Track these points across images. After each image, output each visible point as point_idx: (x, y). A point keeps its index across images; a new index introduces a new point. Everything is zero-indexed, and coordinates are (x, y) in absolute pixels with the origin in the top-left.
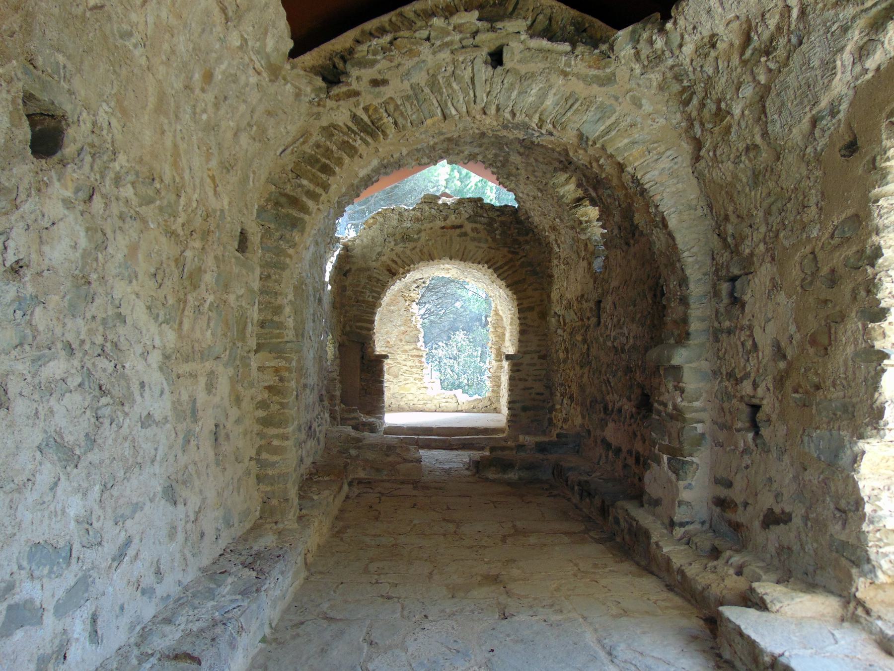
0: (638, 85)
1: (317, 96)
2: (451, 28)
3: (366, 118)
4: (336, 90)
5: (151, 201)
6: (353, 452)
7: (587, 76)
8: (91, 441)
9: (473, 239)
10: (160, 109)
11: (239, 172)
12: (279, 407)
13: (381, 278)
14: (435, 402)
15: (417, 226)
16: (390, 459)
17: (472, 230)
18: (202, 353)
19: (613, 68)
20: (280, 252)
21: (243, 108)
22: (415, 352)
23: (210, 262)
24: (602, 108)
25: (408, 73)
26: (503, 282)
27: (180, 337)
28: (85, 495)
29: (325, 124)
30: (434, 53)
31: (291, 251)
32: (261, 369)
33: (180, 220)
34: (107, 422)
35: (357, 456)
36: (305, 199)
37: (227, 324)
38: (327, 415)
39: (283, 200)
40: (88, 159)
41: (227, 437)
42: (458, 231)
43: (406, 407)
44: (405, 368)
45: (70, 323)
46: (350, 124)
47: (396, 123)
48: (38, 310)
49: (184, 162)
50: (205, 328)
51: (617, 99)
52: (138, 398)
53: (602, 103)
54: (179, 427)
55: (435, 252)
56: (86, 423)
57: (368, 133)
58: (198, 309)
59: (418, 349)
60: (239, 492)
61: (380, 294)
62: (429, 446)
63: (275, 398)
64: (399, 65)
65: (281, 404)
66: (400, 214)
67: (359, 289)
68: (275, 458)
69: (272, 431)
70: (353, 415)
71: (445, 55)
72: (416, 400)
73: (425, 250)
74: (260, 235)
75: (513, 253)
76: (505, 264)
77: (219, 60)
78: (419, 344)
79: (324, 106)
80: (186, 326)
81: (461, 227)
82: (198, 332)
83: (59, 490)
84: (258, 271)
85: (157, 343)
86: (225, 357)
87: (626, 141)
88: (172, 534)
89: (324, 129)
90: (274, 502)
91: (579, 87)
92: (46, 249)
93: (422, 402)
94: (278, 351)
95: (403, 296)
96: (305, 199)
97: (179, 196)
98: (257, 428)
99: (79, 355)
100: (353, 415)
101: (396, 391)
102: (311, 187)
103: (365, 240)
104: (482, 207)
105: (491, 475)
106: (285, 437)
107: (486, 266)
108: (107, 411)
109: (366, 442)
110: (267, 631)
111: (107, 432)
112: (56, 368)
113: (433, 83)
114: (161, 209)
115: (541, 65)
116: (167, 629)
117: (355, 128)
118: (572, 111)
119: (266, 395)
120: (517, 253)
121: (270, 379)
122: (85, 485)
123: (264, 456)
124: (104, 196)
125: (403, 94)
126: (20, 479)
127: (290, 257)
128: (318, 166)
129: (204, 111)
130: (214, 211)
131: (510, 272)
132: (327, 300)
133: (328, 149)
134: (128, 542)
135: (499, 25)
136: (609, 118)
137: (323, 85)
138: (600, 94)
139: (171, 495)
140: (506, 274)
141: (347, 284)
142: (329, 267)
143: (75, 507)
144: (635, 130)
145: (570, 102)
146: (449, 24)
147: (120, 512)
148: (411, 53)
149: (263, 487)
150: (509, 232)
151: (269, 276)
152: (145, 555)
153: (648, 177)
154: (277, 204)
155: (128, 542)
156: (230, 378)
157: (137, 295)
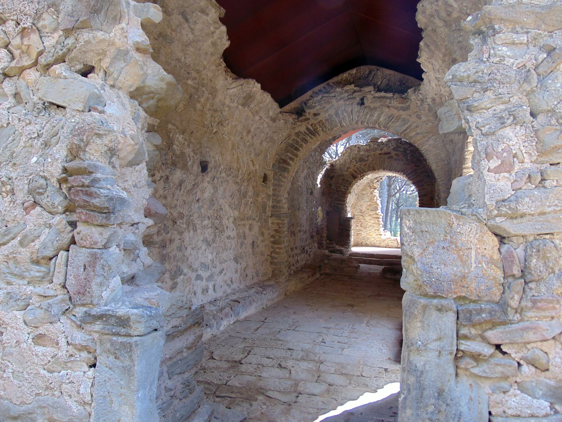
0: (420, 110)
1: (294, 121)
2: (344, 91)
3: (311, 128)
4: (300, 119)
5: (230, 175)
6: (326, 261)
7: (398, 107)
8: (214, 241)
9: (396, 160)
10: (233, 148)
11: (263, 155)
12: (278, 237)
13: (349, 180)
14: (386, 242)
15: (367, 154)
16: (342, 266)
17: (395, 155)
18: (247, 218)
19: (409, 103)
20: (280, 180)
21: (263, 135)
22: (375, 216)
23: (250, 188)
24: (404, 120)
25: (327, 110)
26: (411, 181)
27: (240, 213)
28: (212, 254)
29: (297, 131)
30: (337, 102)
31: (284, 180)
32: (272, 223)
33: (239, 178)
34: (218, 237)
35: (328, 263)
36: (289, 160)
37: (258, 208)
38: (316, 245)
39: (281, 161)
40: (213, 169)
41: (258, 246)
42: (388, 155)
43: (370, 244)
44: (370, 224)
45: (209, 211)
46: (306, 131)
47: (322, 130)
48: (202, 209)
49: (241, 161)
50: (249, 209)
51: (410, 116)
52: (226, 230)
53: (404, 118)
54: (239, 241)
55: (376, 167)
56: (212, 236)
57: (312, 135)
58: (246, 204)
59: (377, 214)
60: (262, 266)
61: (348, 187)
62: (365, 262)
63: (277, 234)
64: (324, 107)
65: (279, 236)
66: (359, 148)
67: (338, 185)
68: (277, 256)
69: (276, 246)
70: (332, 246)
71: (342, 102)
72: (375, 241)
73: (371, 166)
74: (273, 174)
75: (416, 166)
76: (413, 172)
77: (252, 125)
78: (378, 212)
79: (297, 125)
80: (242, 210)
81: (389, 153)
82: (246, 212)
83: (206, 251)
84: (272, 188)
85: (232, 215)
86: (257, 219)
87: (414, 133)
88: (236, 271)
89: (296, 133)
90: (276, 272)
91: (394, 112)
92: (204, 194)
93: (378, 242)
94: (278, 217)
95: (370, 186)
96: (289, 160)
97: (239, 171)
98: (271, 244)
99: (211, 219)
100: (332, 246)
101: (365, 236)
102: (291, 156)
103: (341, 161)
104: (400, 143)
105: (388, 276)
106: (280, 248)
107: (402, 173)
108: (218, 234)
109: (333, 257)
110: (265, 307)
111: (218, 239)
112: (206, 222)
113: (337, 114)
114: (233, 177)
115: (379, 104)
116: (233, 295)
117: (308, 133)
118: (391, 122)
119: (274, 233)
120: (419, 166)
121: (276, 227)
122: (212, 252)
123: (273, 255)
124: (217, 178)
125: (326, 118)
126: (199, 247)
127: (284, 182)
128: (294, 148)
129: (248, 142)
130: (253, 171)
131: (415, 176)
132: (317, 193)
133: (297, 141)
134: (223, 269)
135: (362, 89)
136: (407, 124)
137: (297, 116)
138: (404, 114)
139: (236, 260)
140: (413, 177)
141: (332, 183)
142: (320, 177)
143: (210, 257)
144: (418, 129)
145: (390, 119)
146: (343, 90)
147: (221, 261)
148: (328, 102)
149: (272, 266)
150: (415, 155)
151: (276, 189)
152: (227, 274)
153: (424, 147)
154: (279, 162)
155: (223, 269)
156: (259, 226)
157: (226, 202)
